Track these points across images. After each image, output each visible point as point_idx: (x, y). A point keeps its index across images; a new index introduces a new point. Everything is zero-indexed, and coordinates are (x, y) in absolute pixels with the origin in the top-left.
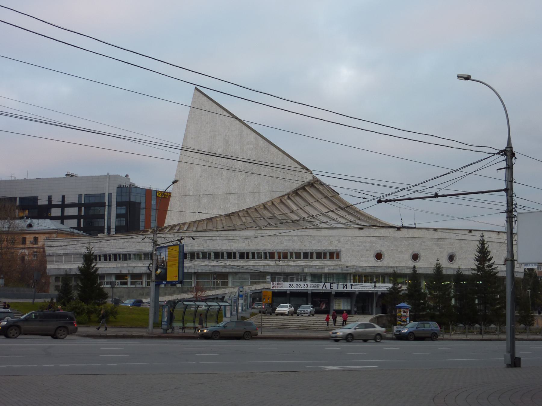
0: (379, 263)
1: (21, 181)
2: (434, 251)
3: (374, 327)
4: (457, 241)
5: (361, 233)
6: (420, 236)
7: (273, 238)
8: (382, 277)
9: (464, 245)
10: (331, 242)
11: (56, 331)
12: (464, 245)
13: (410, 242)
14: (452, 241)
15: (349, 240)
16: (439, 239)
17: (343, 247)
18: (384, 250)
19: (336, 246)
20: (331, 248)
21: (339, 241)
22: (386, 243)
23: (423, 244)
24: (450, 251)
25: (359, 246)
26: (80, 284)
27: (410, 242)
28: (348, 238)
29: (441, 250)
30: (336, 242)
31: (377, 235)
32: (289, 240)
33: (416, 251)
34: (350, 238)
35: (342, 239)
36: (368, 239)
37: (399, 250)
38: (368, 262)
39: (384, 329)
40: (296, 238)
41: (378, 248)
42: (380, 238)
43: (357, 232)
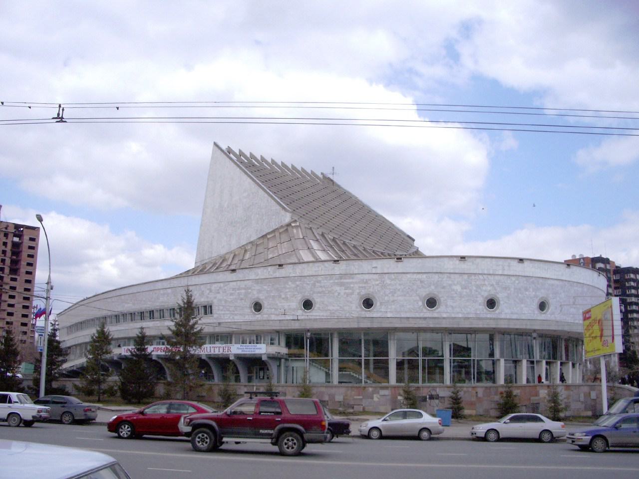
0: (258, 316)
1: (605, 259)
2: (336, 294)
3: (541, 420)
4: (376, 277)
5: (233, 276)
6: (311, 273)
7: (151, 293)
8: (257, 336)
9: (388, 282)
10: (203, 293)
11: (62, 416)
12: (388, 282)
13: (298, 283)
14: (366, 277)
15: (220, 288)
16: (342, 276)
17: (215, 298)
18: (262, 298)
19: (207, 297)
20: (202, 300)
21: (211, 291)
22: (265, 287)
23: (317, 284)
24: (363, 292)
25: (231, 294)
26: (146, 366)
27: (298, 283)
28: (219, 285)
29: (347, 291)
30: (208, 292)
31: (253, 277)
32: (164, 294)
33: (307, 295)
34: (222, 285)
35: (214, 287)
36: (242, 285)
37: (283, 296)
38: (243, 317)
39: (436, 420)
40: (169, 291)
41: (256, 294)
42: (257, 281)
43: (229, 276)
